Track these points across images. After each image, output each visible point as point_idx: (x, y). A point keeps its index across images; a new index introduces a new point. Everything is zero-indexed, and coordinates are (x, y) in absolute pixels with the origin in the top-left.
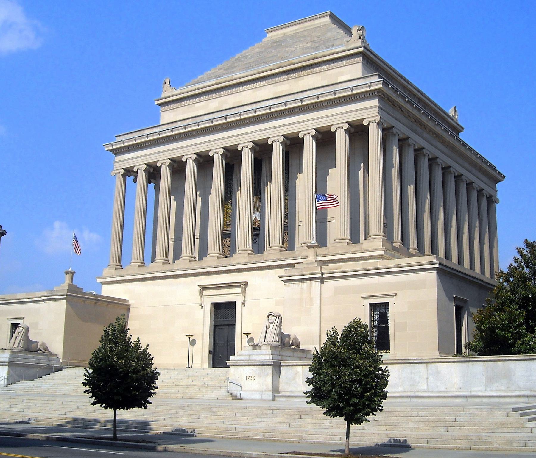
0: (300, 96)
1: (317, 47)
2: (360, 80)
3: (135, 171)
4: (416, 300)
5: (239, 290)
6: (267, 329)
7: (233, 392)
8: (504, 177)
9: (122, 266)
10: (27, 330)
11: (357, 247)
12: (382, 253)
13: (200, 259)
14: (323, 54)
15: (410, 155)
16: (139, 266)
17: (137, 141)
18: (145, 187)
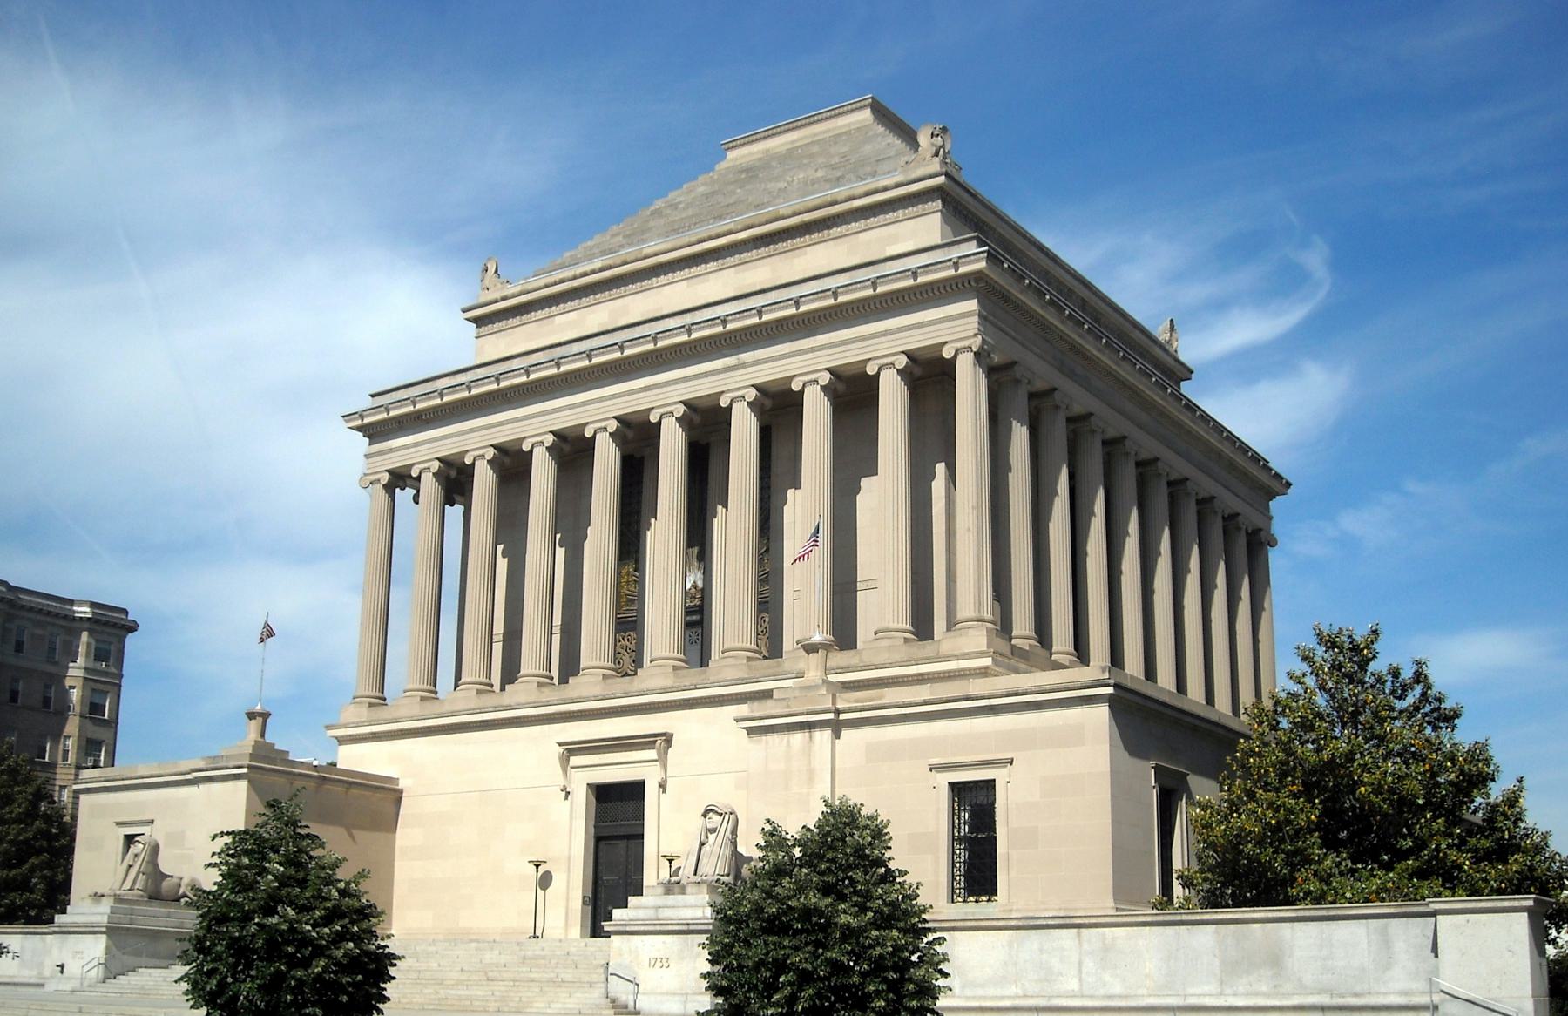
2: (938, 251)
3: (414, 474)
4: (1064, 774)
5: (651, 754)
6: (702, 844)
8: (1289, 485)
10: (155, 850)
11: (927, 648)
12: (987, 662)
13: (564, 680)
15: (1058, 434)
17: (419, 406)
18: (436, 513)
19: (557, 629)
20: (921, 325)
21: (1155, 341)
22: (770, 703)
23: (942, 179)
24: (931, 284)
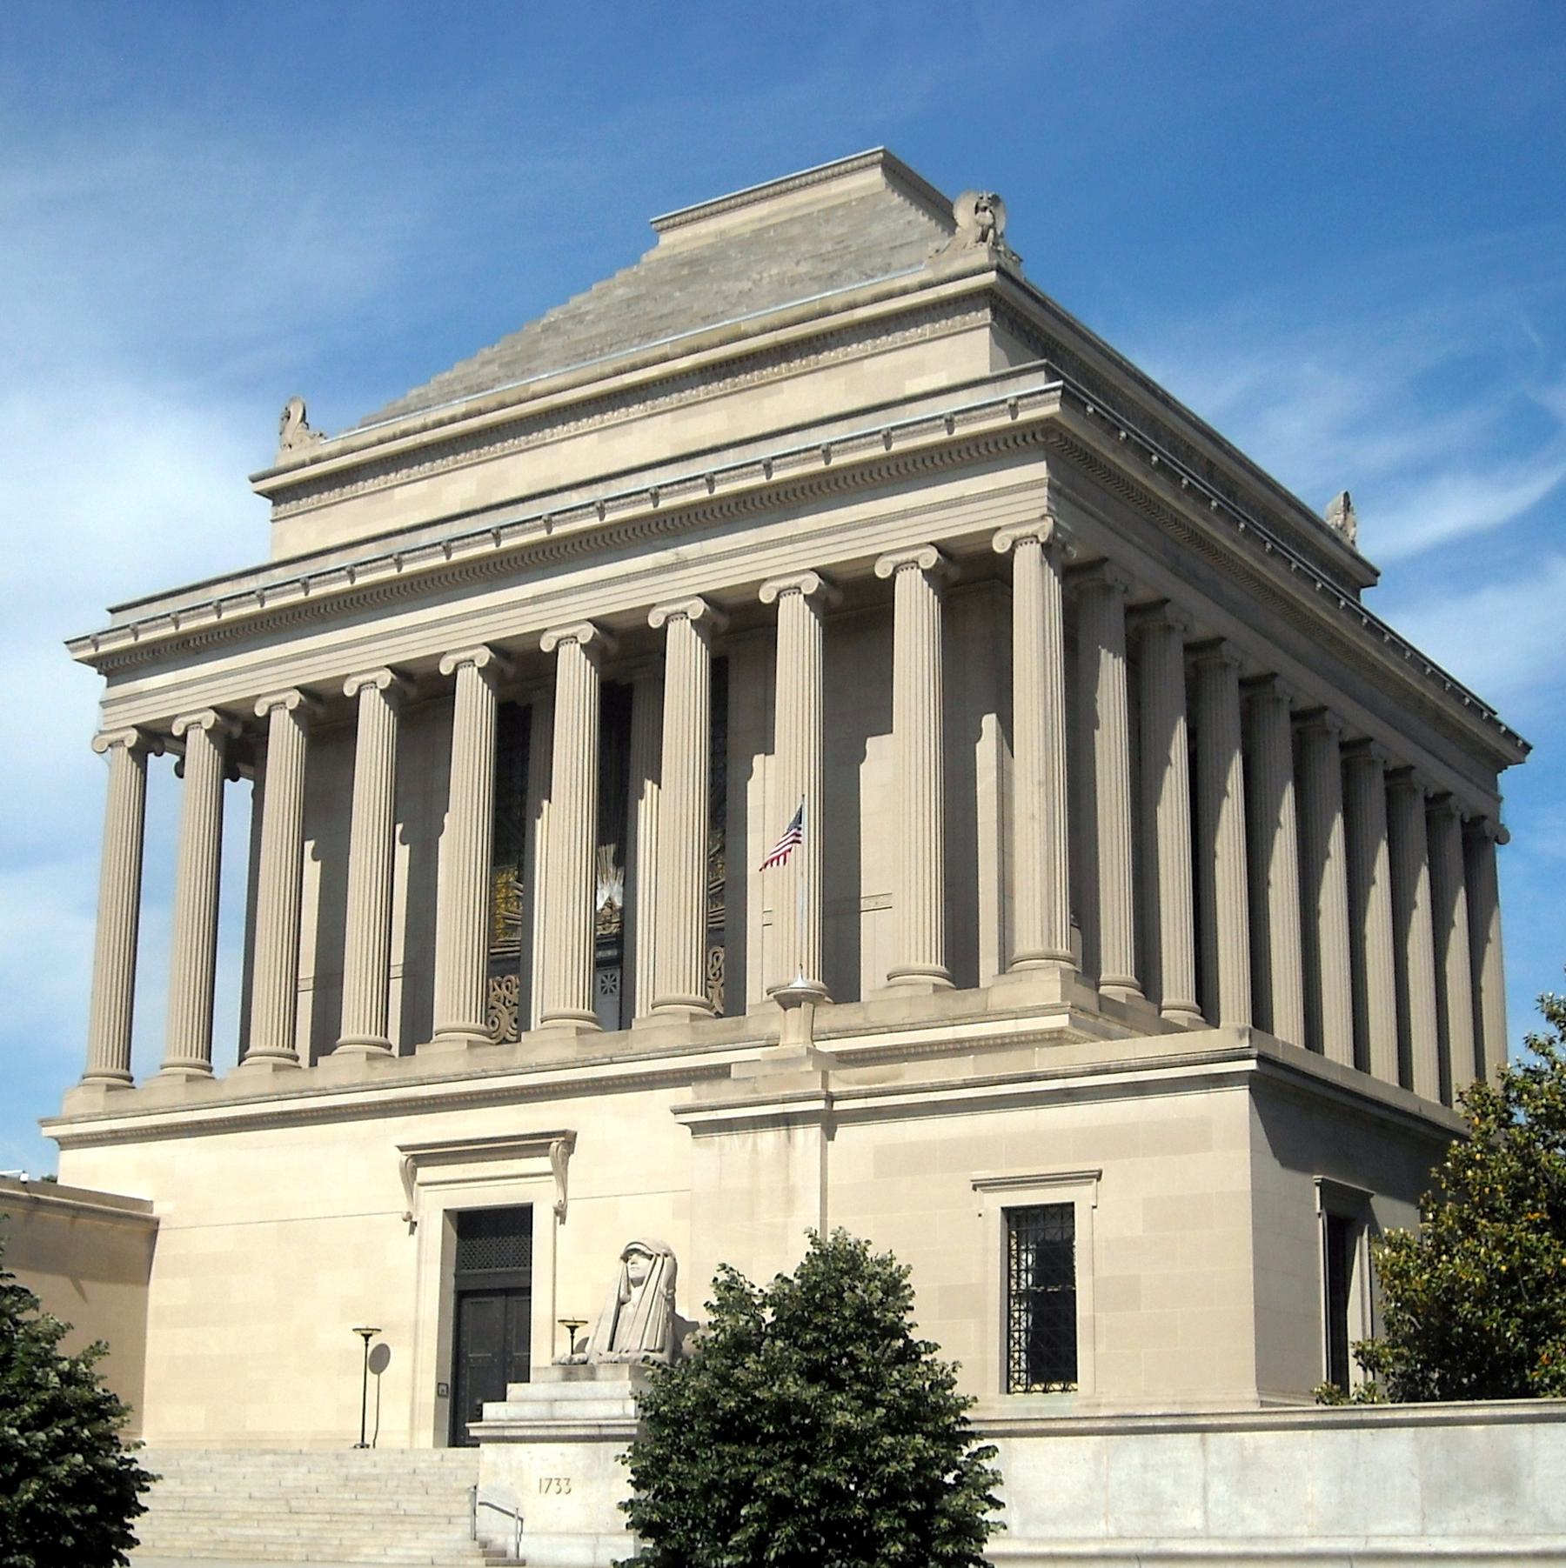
0: (765, 451)
1: (831, 276)
3: (177, 731)
4: (1180, 1196)
5: (543, 1164)
6: (621, 1303)
7: (492, 1536)
8: (1527, 748)
9: (131, 1079)
11: (969, 1000)
12: (1062, 1021)
13: (407, 1049)
14: (850, 298)
15: (1170, 668)
16: (190, 1079)
18: (210, 791)
19: (396, 971)
20: (960, 501)
21: (1321, 526)
22: (726, 1085)
23: (992, 276)
24: (975, 439)
